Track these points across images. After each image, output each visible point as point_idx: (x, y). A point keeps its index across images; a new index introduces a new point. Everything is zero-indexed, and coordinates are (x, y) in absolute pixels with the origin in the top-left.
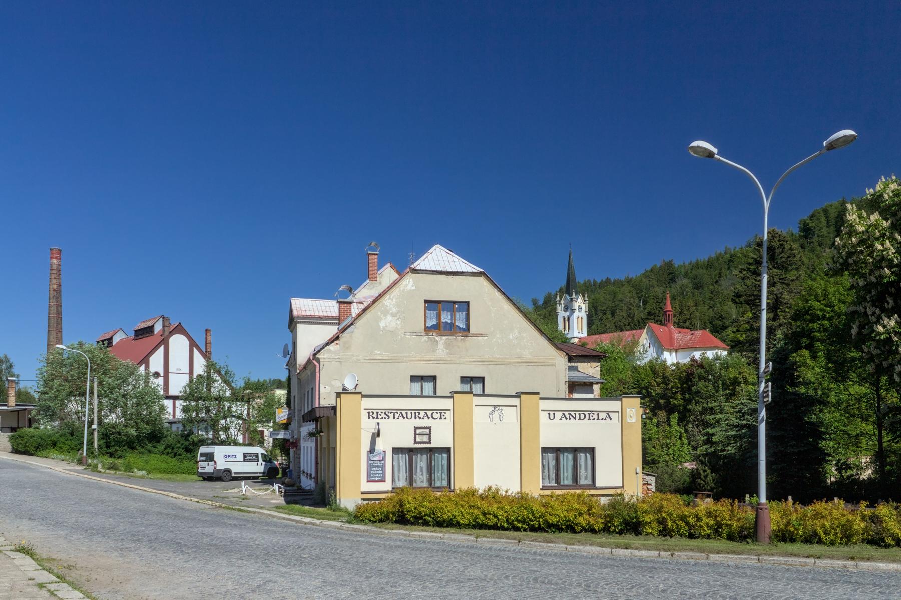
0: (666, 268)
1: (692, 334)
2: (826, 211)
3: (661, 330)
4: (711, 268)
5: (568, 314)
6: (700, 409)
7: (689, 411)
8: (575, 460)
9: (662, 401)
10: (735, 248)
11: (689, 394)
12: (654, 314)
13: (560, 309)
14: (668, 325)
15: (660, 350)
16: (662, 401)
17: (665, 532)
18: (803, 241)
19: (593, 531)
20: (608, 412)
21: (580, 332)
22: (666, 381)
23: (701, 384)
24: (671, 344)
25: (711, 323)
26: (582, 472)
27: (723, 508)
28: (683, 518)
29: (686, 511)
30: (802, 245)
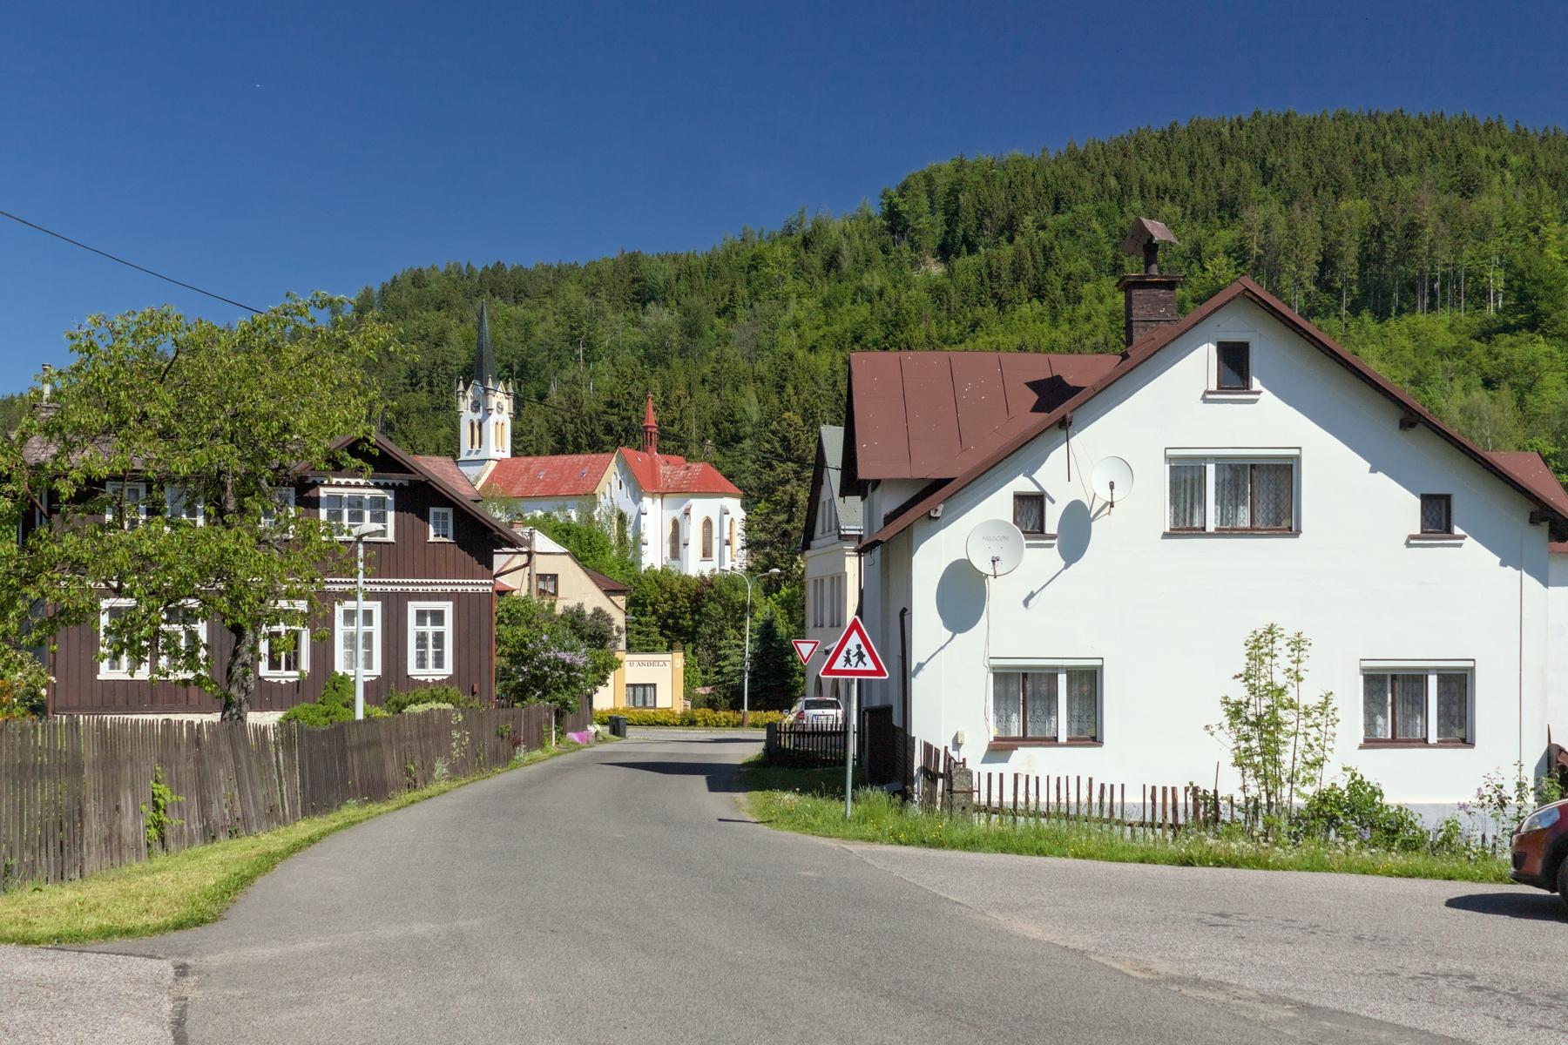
0: (627, 269)
1: (688, 468)
2: (929, 179)
3: (639, 458)
4: (715, 277)
5: (479, 415)
6: (709, 632)
7: (698, 632)
8: (645, 691)
9: (670, 621)
10: (763, 230)
11: (699, 615)
12: (618, 405)
13: (465, 406)
14: (650, 449)
15: (637, 494)
16: (670, 621)
17: (706, 725)
18: (888, 237)
19: (676, 725)
20: (664, 662)
21: (500, 449)
22: (674, 598)
23: (711, 605)
24: (655, 485)
25: (715, 424)
26: (648, 699)
27: (730, 714)
28: (714, 719)
29: (715, 715)
30: (884, 246)
